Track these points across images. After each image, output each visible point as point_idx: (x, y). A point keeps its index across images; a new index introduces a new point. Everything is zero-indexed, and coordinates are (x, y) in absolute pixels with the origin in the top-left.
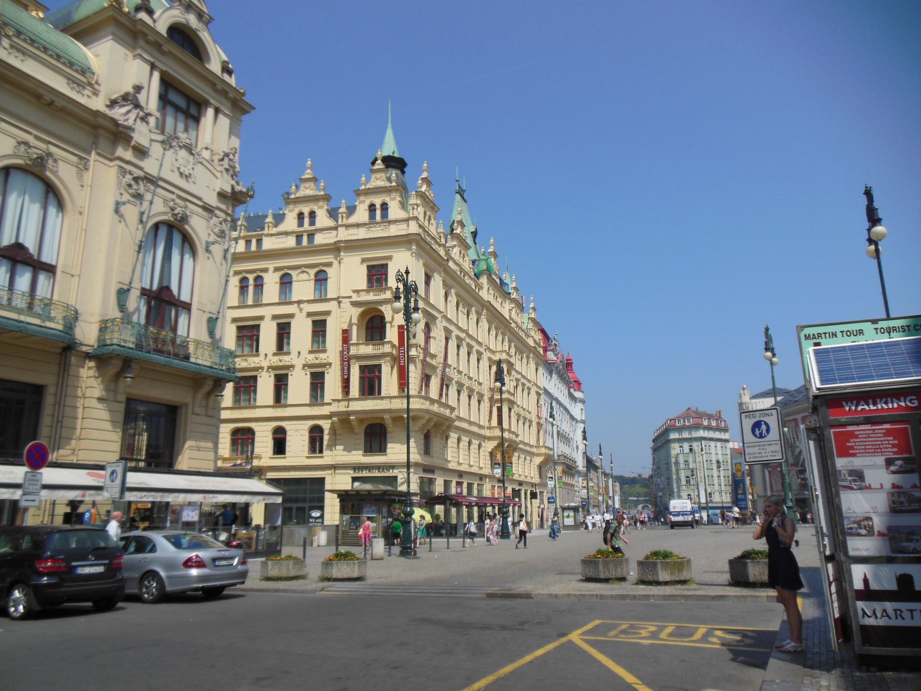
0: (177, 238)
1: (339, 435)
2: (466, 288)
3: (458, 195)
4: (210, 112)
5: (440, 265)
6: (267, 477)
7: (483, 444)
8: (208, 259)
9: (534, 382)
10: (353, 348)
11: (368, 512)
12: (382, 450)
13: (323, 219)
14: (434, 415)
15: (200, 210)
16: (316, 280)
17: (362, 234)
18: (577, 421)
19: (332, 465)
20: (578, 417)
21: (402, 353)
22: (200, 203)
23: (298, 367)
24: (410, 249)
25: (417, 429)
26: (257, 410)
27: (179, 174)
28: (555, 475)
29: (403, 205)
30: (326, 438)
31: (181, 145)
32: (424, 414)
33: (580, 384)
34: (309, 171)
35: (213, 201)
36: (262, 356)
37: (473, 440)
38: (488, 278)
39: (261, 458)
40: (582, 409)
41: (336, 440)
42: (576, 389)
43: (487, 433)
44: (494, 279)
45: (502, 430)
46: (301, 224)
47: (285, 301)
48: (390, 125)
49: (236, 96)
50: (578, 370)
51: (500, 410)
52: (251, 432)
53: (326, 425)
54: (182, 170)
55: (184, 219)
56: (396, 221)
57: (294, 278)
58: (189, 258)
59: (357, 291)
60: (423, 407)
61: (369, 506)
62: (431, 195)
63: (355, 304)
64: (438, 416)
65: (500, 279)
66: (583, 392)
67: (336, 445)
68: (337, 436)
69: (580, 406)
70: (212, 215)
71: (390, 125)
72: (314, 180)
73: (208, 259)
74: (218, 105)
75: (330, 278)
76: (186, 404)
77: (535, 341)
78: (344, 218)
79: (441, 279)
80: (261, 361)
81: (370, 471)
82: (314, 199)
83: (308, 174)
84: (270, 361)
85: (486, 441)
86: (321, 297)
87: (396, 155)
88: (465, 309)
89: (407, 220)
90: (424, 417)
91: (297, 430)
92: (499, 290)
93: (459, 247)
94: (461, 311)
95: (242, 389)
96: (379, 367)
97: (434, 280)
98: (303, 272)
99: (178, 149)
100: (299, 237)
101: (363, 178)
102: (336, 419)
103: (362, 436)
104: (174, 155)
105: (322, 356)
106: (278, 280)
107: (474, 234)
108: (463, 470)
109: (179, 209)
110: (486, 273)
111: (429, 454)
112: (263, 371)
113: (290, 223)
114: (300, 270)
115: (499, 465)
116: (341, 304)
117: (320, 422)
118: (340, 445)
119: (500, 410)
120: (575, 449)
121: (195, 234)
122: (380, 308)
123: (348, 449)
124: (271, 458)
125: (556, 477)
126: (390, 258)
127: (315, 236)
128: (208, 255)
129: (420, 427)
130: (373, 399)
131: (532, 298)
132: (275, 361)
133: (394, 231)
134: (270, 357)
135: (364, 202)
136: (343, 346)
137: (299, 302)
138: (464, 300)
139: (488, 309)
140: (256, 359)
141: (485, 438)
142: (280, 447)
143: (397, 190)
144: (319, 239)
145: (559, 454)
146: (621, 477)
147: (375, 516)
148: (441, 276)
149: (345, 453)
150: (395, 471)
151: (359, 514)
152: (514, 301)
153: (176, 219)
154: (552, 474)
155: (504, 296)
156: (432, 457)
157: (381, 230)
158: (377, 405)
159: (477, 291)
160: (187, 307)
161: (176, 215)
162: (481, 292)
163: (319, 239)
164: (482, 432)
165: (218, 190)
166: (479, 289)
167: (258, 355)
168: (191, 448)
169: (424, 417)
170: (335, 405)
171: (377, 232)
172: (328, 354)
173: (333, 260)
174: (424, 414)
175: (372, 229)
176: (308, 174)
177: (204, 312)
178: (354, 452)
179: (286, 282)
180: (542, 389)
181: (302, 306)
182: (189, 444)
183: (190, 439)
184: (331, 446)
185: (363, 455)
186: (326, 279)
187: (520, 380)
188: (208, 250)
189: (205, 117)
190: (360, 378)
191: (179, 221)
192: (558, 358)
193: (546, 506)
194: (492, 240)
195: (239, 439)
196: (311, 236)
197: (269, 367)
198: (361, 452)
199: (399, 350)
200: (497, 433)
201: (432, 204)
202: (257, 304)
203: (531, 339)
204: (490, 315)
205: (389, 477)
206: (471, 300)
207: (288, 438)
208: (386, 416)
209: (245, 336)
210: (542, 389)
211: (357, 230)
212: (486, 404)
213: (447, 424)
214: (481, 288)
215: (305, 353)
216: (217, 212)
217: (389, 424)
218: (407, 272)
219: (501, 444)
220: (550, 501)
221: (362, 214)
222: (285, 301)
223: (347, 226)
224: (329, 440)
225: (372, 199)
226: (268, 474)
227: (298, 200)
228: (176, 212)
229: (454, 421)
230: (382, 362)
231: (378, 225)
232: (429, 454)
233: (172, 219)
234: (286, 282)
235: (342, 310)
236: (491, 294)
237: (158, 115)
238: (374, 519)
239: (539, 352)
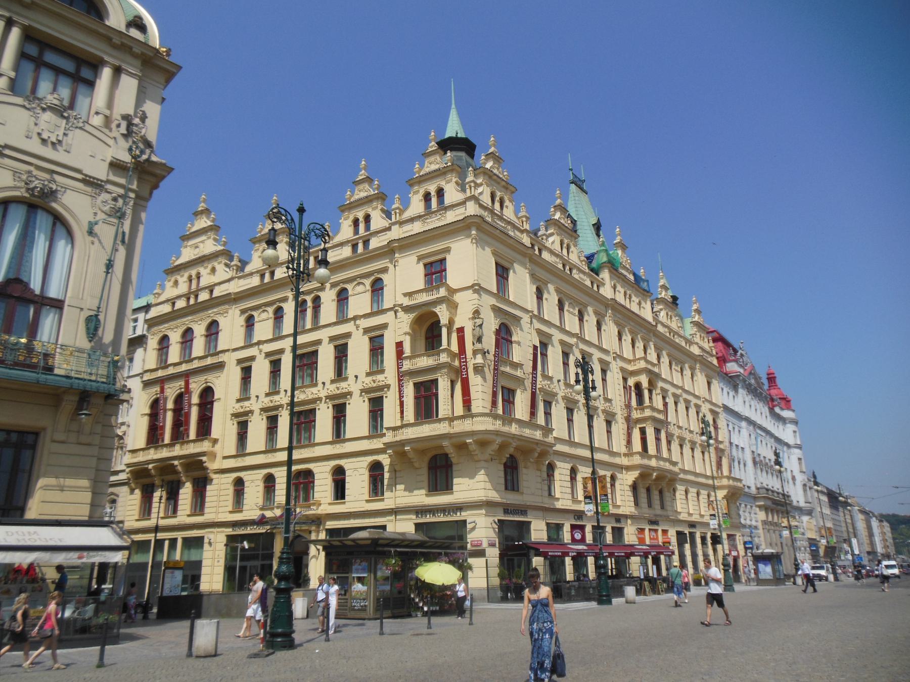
0: (43, 221)
1: (400, 471)
2: (578, 286)
3: (573, 186)
4: (106, 73)
5: (524, 255)
6: (327, 527)
7: (619, 476)
8: (93, 243)
9: (704, 398)
10: (406, 363)
11: (357, 571)
12: (447, 487)
13: (378, 221)
14: (513, 438)
15: (80, 185)
16: (373, 291)
17: (417, 227)
18: (788, 446)
19: (392, 509)
20: (791, 441)
21: (463, 362)
22: (80, 176)
23: (356, 393)
24: (469, 236)
25: (487, 456)
26: (317, 448)
27: (40, 141)
28: (718, 513)
29: (462, 187)
30: (387, 475)
31: (45, 106)
32: (493, 437)
33: (789, 401)
34: (363, 171)
35: (101, 172)
36: (320, 386)
37: (580, 467)
38: (610, 272)
39: (320, 504)
40: (795, 432)
41: (396, 478)
42: (784, 407)
43: (625, 461)
44: (621, 274)
45: (592, 448)
46: (356, 232)
47: (342, 319)
48: (453, 106)
49: (145, 51)
50: (785, 386)
51: (643, 431)
52: (309, 474)
53: (385, 460)
54: (45, 136)
55: (52, 194)
56: (453, 206)
57: (350, 293)
58: (293, 301)
59: (409, 295)
60: (491, 427)
61: (358, 561)
62: (504, 174)
63: (407, 309)
64: (519, 440)
65: (634, 274)
66: (793, 411)
67: (396, 485)
68: (397, 473)
69: (791, 428)
70: (101, 191)
71: (453, 106)
72: (369, 180)
73: (93, 243)
74: (117, 63)
75: (386, 285)
76: (44, 429)
77: (701, 348)
78: (398, 215)
79: (527, 271)
80: (319, 391)
81: (434, 515)
82: (368, 200)
83: (362, 174)
84: (328, 389)
85: (624, 472)
86: (378, 308)
87: (461, 135)
88: (574, 309)
89: (463, 203)
90: (494, 441)
91: (355, 469)
92: (633, 287)
93: (558, 235)
94: (568, 311)
95: (303, 425)
96: (435, 382)
97: (514, 272)
98: (359, 284)
99: (40, 111)
100: (355, 247)
101: (417, 166)
102: (391, 451)
103: (425, 471)
104: (33, 119)
105: (380, 377)
106: (335, 297)
107: (596, 226)
108: (621, 513)
109: (36, 182)
110: (608, 266)
111: (518, 491)
112: (321, 403)
113: (346, 232)
114: (356, 283)
115: (591, 499)
116: (398, 314)
117: (342, 462)
118: (400, 484)
119: (643, 431)
120: (791, 481)
121: (70, 213)
122: (434, 310)
123: (409, 489)
124: (367, 501)
125: (720, 515)
126: (448, 250)
127: (370, 241)
128: (91, 238)
129: (507, 458)
130: (429, 423)
131: (694, 299)
132: (332, 389)
133: (451, 217)
134: (328, 385)
135: (418, 191)
136: (398, 362)
137: (355, 318)
138: (570, 298)
139: (614, 309)
140: (314, 390)
141: (621, 468)
142: (340, 491)
143: (452, 171)
144: (374, 243)
145: (759, 486)
146: (894, 516)
147: (365, 575)
148: (526, 269)
149: (407, 493)
150: (463, 514)
151: (348, 573)
152: (663, 301)
153: (33, 195)
154: (714, 510)
155: (644, 295)
156: (522, 493)
157: (437, 220)
158: (434, 430)
159: (595, 288)
160: (58, 305)
161: (33, 189)
162: (602, 291)
163: (374, 243)
164: (617, 460)
165: (109, 159)
166: (598, 286)
167: (316, 385)
168: (46, 488)
169: (494, 441)
170: (389, 434)
171: (434, 222)
172: (385, 375)
173: (389, 265)
174: (493, 437)
175: (428, 221)
176: (361, 175)
177: (82, 309)
178: (416, 492)
179: (342, 297)
180: (719, 407)
181: (358, 322)
182: (41, 482)
183: (44, 476)
184: (393, 484)
185: (427, 495)
186: (382, 289)
187: (681, 396)
188: (91, 232)
189: (100, 78)
190: (416, 398)
191: (39, 197)
192: (745, 370)
193: (742, 553)
194: (618, 230)
195: (301, 483)
196: (366, 243)
197: (327, 397)
198: (423, 492)
199: (460, 358)
200: (637, 460)
201: (504, 183)
202: (316, 327)
203: (695, 346)
204: (618, 316)
205: (457, 521)
206: (584, 298)
207: (348, 479)
208: (445, 443)
209: (305, 365)
210: (719, 407)
211: (411, 225)
212: (619, 428)
213: (539, 450)
214: (600, 284)
215: (262, 396)
216: (109, 187)
217: (452, 453)
218: (301, 210)
219: (643, 476)
220: (747, 546)
221: (416, 206)
222: (342, 319)
223: (401, 223)
224: (389, 479)
225: (425, 187)
226: (328, 523)
227: (352, 205)
228: (31, 186)
229: (551, 445)
230: (438, 375)
231: (434, 215)
232: (518, 491)
233: (27, 195)
234: (342, 297)
235: (399, 320)
236: (619, 292)
237: (12, 74)
238: (366, 581)
239: (711, 363)
